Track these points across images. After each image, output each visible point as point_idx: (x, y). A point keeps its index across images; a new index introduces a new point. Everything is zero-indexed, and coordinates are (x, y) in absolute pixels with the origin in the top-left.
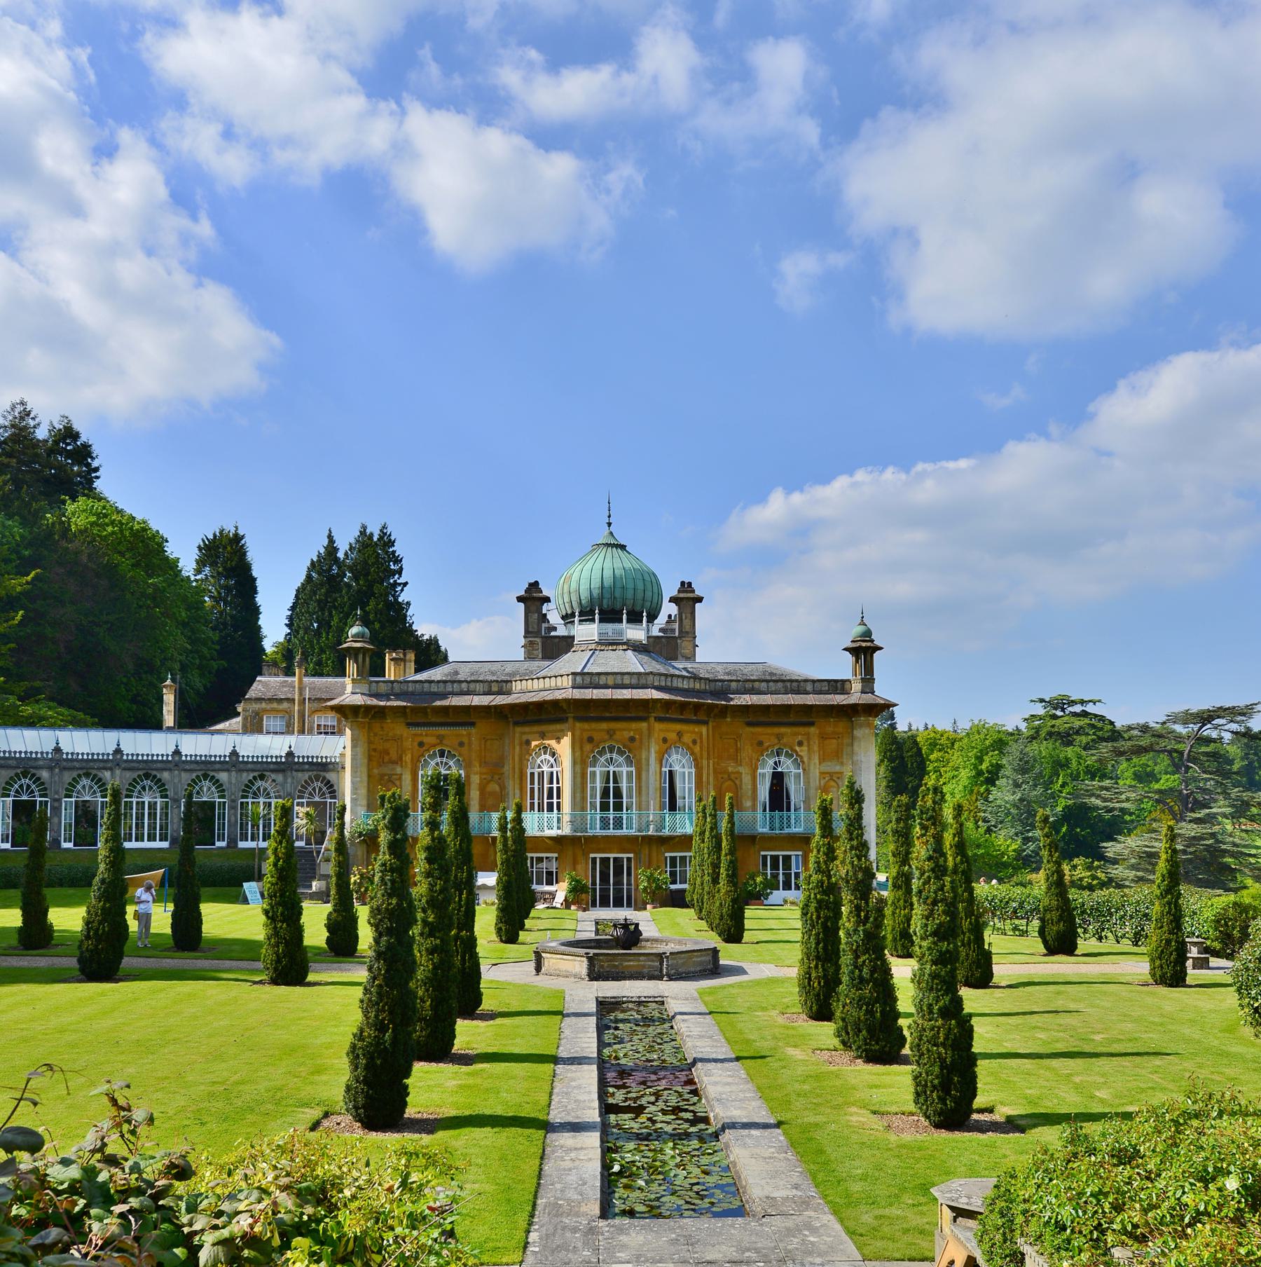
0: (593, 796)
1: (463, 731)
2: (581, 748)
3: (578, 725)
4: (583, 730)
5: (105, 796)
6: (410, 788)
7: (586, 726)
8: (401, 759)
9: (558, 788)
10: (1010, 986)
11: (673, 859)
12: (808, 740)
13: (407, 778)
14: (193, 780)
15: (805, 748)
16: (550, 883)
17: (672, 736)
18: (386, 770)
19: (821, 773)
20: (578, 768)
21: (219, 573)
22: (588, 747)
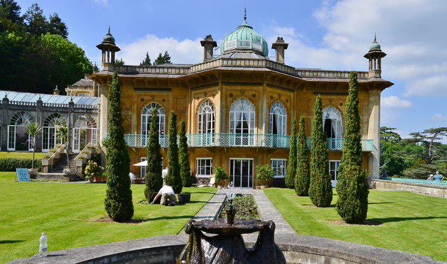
0: (232, 126)
1: (165, 93)
2: (226, 100)
7: (229, 88)
9: (213, 122)
10: (198, 202)
11: (275, 162)
14: (49, 117)
16: (208, 173)
17: (276, 96)
20: (224, 110)
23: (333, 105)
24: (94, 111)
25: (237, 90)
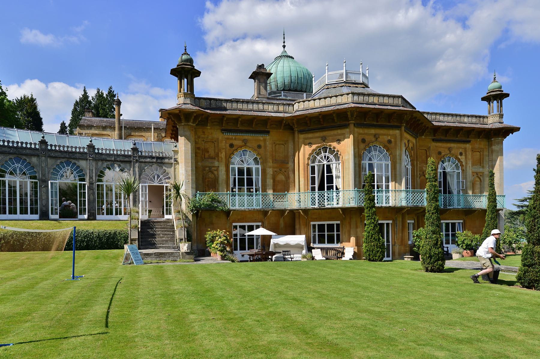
1: (260, 137)
3: (356, 130)
4: (360, 134)
5: (83, 180)
6: (225, 177)
7: (361, 131)
8: (217, 155)
12: (466, 152)
13: (222, 169)
15: (463, 157)
18: (207, 164)
19: (473, 172)
21: (24, 115)
22: (362, 146)
23: (453, 155)
24: (166, 161)
25: (371, 134)
